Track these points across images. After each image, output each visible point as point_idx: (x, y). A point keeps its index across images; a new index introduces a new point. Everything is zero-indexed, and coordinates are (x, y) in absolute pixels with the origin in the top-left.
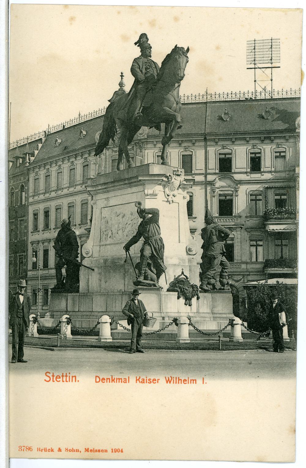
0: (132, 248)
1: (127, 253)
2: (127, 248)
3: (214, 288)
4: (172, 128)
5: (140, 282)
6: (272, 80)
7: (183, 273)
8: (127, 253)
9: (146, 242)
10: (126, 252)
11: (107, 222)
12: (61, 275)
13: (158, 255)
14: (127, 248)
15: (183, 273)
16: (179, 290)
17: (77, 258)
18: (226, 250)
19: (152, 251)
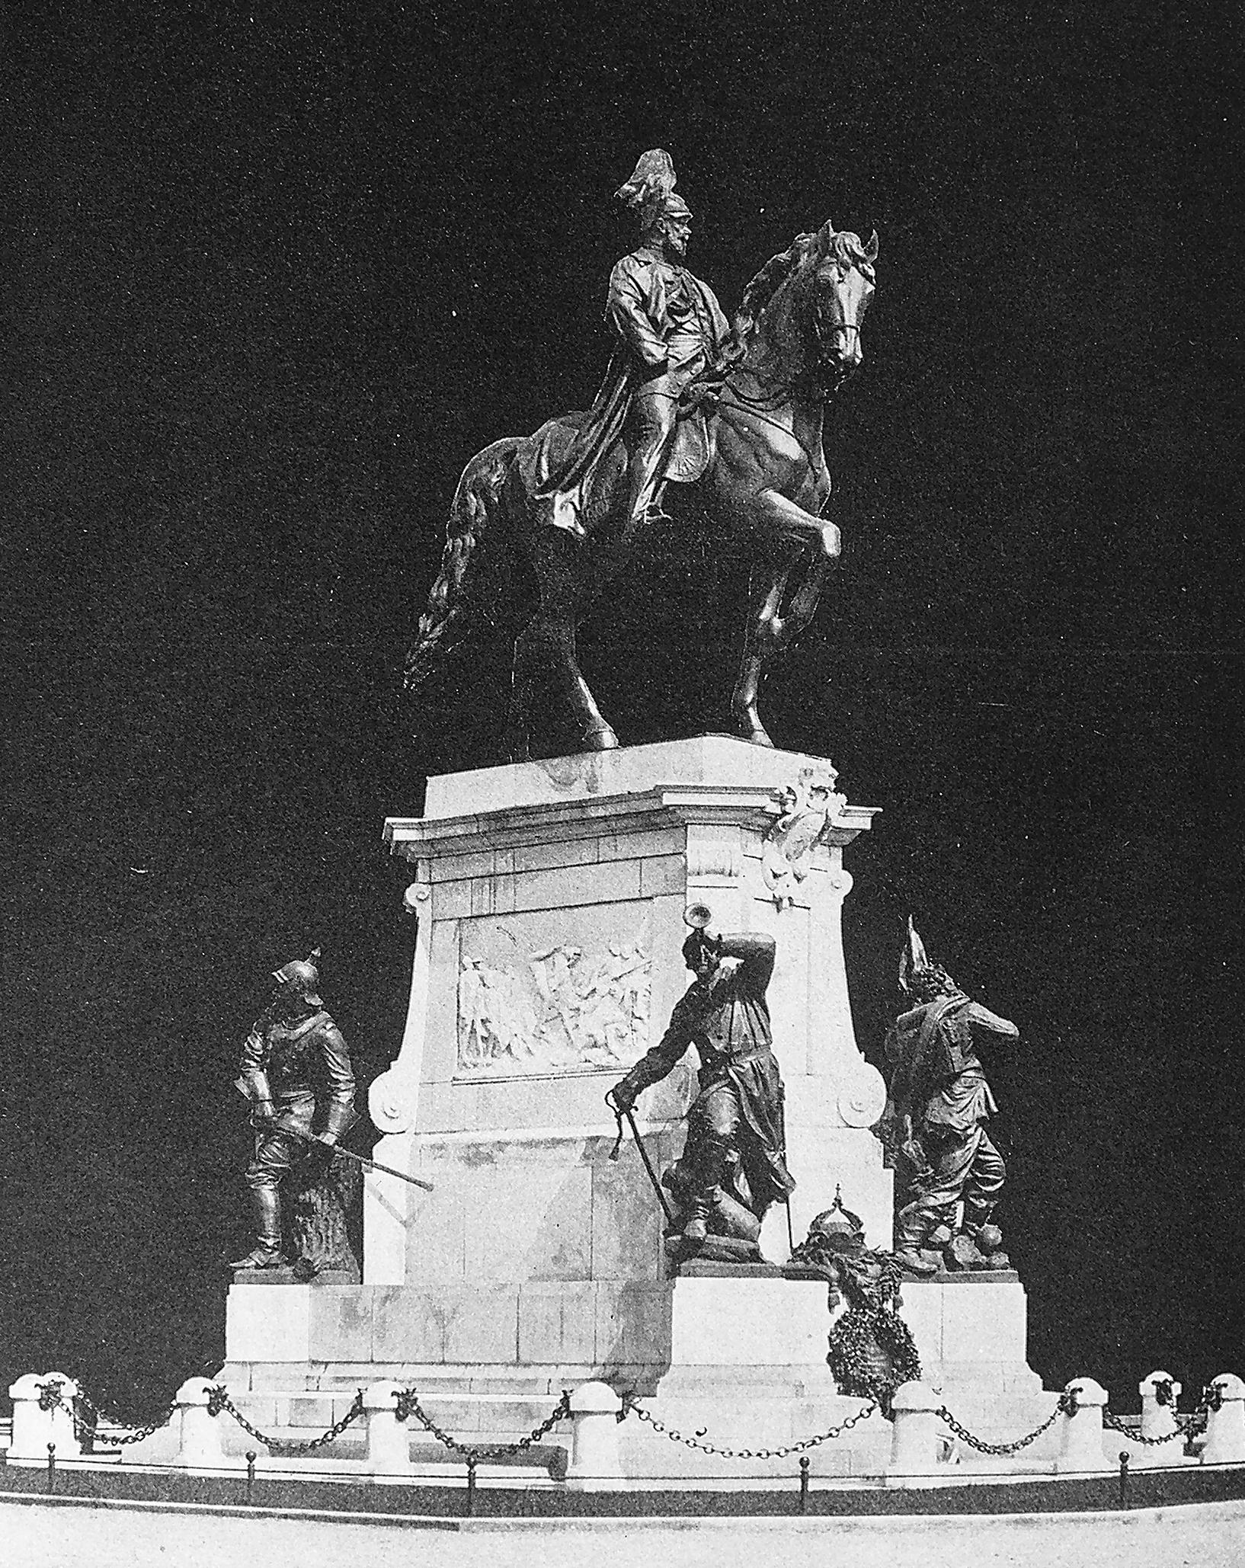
0: (647, 1100)
1: (624, 1117)
2: (624, 1099)
3: (952, 1264)
4: (619, 413)
5: (699, 1243)
6: (307, 1390)
7: (838, 1203)
8: (624, 1117)
9: (713, 1069)
10: (618, 1116)
11: (438, 1153)
12: (656, 484)
13: (766, 1130)
14: (624, 1099)
15: (838, 1203)
16: (834, 1273)
17: (984, 1117)
18: (997, 1105)
19: (741, 1115)
